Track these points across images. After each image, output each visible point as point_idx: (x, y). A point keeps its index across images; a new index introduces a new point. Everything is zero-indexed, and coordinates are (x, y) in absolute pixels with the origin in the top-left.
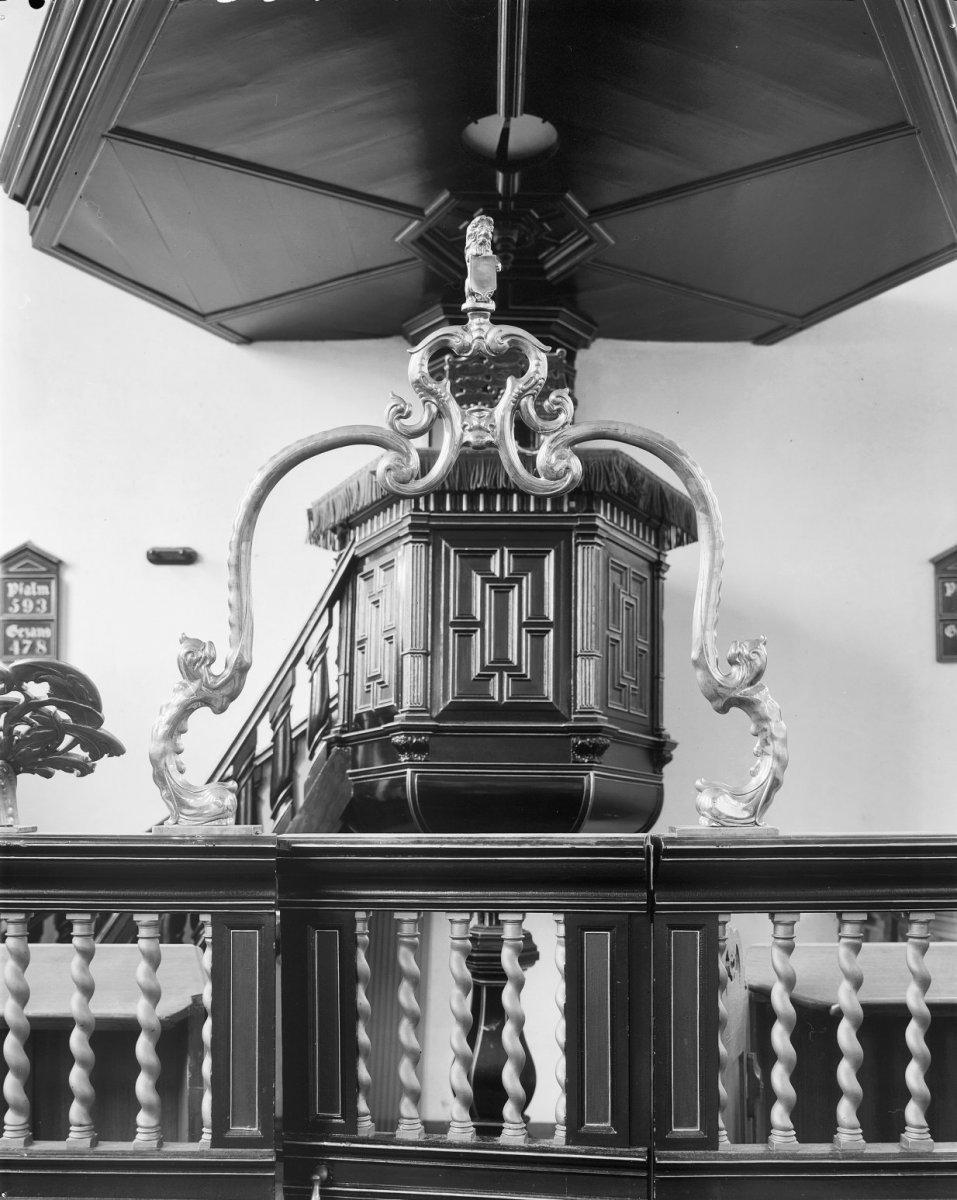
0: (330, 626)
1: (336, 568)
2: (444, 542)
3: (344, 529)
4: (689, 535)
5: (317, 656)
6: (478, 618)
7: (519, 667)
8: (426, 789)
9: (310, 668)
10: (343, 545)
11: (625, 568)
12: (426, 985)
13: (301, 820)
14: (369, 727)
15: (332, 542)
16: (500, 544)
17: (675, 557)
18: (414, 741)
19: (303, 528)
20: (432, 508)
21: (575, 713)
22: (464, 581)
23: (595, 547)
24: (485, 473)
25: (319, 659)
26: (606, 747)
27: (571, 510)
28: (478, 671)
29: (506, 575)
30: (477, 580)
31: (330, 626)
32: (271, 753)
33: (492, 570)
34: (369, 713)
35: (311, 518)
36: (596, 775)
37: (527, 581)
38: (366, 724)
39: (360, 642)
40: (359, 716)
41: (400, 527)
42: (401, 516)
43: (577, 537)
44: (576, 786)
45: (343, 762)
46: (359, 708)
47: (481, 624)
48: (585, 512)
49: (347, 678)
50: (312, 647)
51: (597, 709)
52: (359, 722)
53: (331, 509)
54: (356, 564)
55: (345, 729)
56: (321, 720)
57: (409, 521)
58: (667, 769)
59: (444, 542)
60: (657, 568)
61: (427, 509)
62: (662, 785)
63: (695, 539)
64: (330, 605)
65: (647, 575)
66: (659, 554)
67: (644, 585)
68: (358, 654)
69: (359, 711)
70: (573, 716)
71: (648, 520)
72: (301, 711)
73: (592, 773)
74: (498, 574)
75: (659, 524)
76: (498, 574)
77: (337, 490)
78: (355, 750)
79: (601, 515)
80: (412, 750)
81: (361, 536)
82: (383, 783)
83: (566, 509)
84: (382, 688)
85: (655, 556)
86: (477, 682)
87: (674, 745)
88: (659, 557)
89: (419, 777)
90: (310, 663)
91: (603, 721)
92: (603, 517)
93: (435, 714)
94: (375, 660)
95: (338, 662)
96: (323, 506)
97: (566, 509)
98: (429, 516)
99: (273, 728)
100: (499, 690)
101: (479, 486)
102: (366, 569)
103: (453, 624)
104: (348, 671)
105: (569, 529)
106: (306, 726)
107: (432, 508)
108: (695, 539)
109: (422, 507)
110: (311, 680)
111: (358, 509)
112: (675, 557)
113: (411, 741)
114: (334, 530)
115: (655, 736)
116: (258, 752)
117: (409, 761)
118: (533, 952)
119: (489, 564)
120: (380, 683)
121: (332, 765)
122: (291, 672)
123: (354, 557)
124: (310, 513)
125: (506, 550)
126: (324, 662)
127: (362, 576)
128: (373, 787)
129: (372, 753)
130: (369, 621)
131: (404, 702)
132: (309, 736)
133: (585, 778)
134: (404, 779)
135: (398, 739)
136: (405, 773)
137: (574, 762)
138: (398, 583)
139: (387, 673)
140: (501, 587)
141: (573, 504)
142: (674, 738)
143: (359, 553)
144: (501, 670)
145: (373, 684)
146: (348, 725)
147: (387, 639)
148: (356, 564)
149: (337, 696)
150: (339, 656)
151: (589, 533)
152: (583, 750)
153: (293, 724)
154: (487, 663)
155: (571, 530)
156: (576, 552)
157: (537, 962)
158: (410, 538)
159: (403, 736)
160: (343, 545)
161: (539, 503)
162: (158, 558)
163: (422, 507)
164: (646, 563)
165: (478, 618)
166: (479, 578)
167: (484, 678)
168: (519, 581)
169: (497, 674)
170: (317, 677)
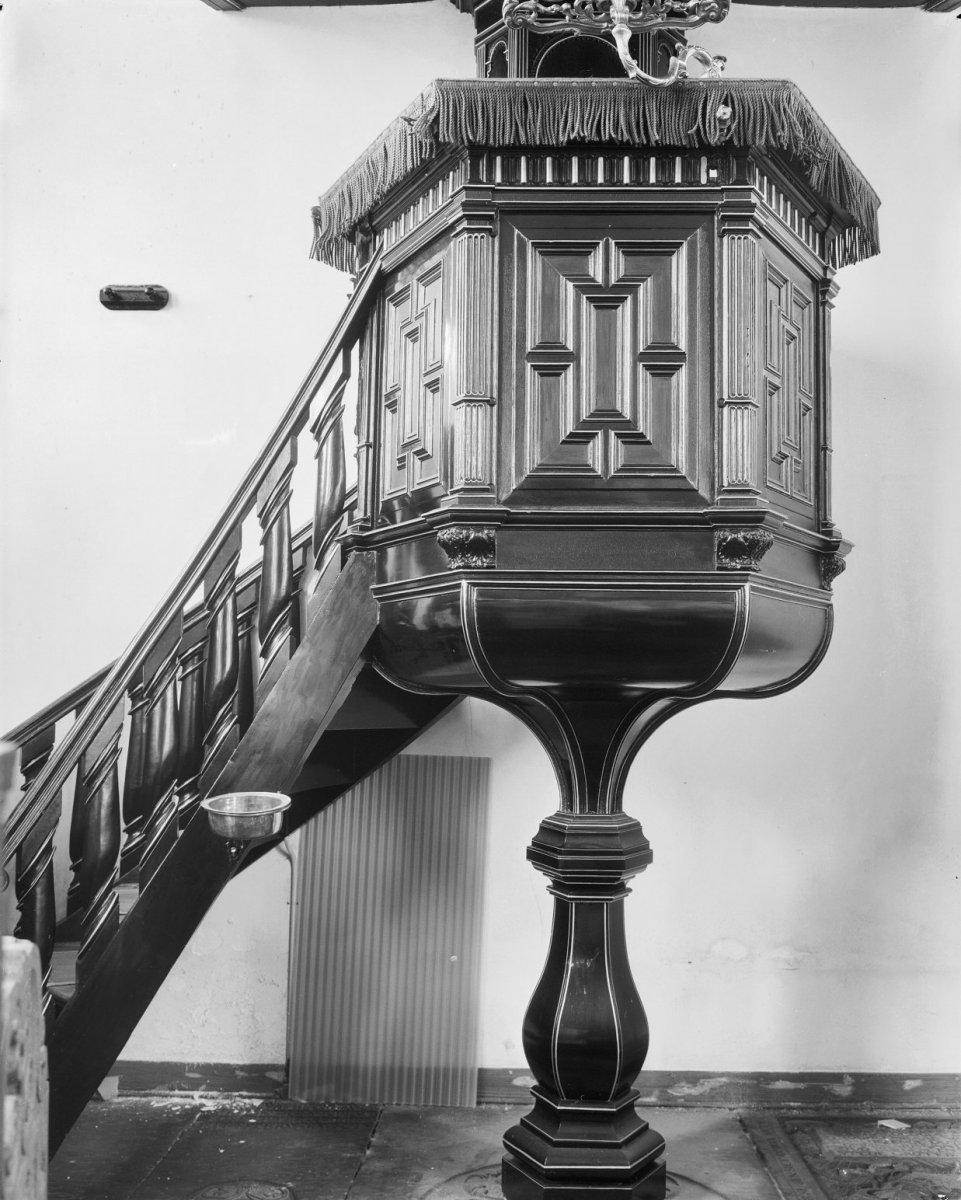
0: (346, 375)
1: (353, 292)
2: (516, 231)
3: (366, 228)
4: (870, 245)
5: (326, 420)
6: (570, 346)
7: (633, 423)
8: (490, 619)
9: (317, 438)
10: (365, 259)
11: (786, 281)
12: (483, 882)
13: (304, 658)
14: (403, 520)
15: (350, 260)
16: (602, 232)
17: (845, 277)
18: (472, 536)
19: (306, 234)
20: (498, 179)
21: (720, 493)
22: (547, 292)
23: (749, 237)
24: (582, 117)
25: (330, 423)
26: (769, 545)
27: (710, 181)
28: (570, 429)
29: (613, 281)
30: (568, 289)
31: (346, 375)
32: (259, 572)
33: (562, 339)
34: (402, 499)
35: (317, 222)
36: (753, 589)
37: (646, 290)
38: (398, 515)
39: (388, 397)
40: (388, 503)
41: (452, 208)
42: (450, 193)
43: (724, 219)
44: (728, 606)
45: (364, 573)
46: (388, 489)
47: (574, 357)
48: (732, 184)
49: (371, 451)
50: (318, 407)
51: (753, 485)
52: (388, 512)
53: (347, 199)
54: (383, 281)
55: (369, 522)
56: (331, 516)
57: (462, 197)
58: (837, 583)
59: (516, 231)
60: (822, 287)
61: (491, 179)
62: (831, 605)
63: (875, 250)
64: (346, 346)
65: (810, 297)
66: (825, 269)
67: (807, 310)
68: (387, 416)
69: (387, 498)
70: (718, 498)
71: (813, 215)
72: (302, 513)
73: (747, 586)
74: (600, 279)
75: (825, 225)
76: (600, 279)
77: (354, 168)
78: (383, 558)
79: (757, 188)
80: (579, 143)
81: (392, 240)
82: (423, 605)
83: (704, 180)
84: (422, 459)
85: (821, 272)
86: (566, 446)
87: (850, 546)
88: (825, 274)
89: (480, 594)
90: (317, 430)
91: (763, 503)
92: (761, 194)
93: (504, 497)
94: (418, 416)
95: (357, 432)
96: (335, 199)
97: (704, 180)
98: (493, 190)
99: (264, 524)
100: (603, 456)
101: (572, 137)
102: (398, 287)
103: (532, 356)
104: (371, 440)
105: (709, 212)
106: (311, 533)
107: (498, 179)
108: (875, 250)
109: (483, 177)
110: (319, 455)
111: (386, 189)
112: (845, 277)
113: (468, 537)
114: (351, 238)
115: (823, 533)
116: (239, 572)
117: (463, 567)
118: (643, 853)
119: (587, 264)
120: (417, 453)
121: (349, 579)
122: (288, 446)
123: (380, 272)
124: (316, 213)
125: (612, 243)
126: (337, 427)
127: (390, 300)
128: (408, 611)
129: (408, 564)
130: (402, 363)
131: (457, 475)
132: (316, 545)
133: (738, 593)
134: (457, 597)
135: (445, 535)
136: (458, 586)
137: (719, 569)
138: (442, 328)
139: (429, 437)
140: (606, 299)
141: (714, 174)
142: (845, 537)
143: (387, 265)
144: (606, 427)
145: (409, 454)
146: (372, 519)
147: (428, 385)
148: (383, 281)
149: (355, 490)
150: (359, 420)
151: (740, 219)
152: (733, 550)
153: (295, 529)
154: (584, 416)
155: (713, 213)
156: (721, 245)
157: (649, 866)
158: (465, 224)
159: (453, 530)
160: (365, 259)
161: (663, 173)
162: (155, 299)
163: (483, 177)
164: (809, 281)
165: (570, 346)
166: (570, 285)
167: (580, 438)
168: (633, 290)
169: (600, 433)
170: (328, 450)
